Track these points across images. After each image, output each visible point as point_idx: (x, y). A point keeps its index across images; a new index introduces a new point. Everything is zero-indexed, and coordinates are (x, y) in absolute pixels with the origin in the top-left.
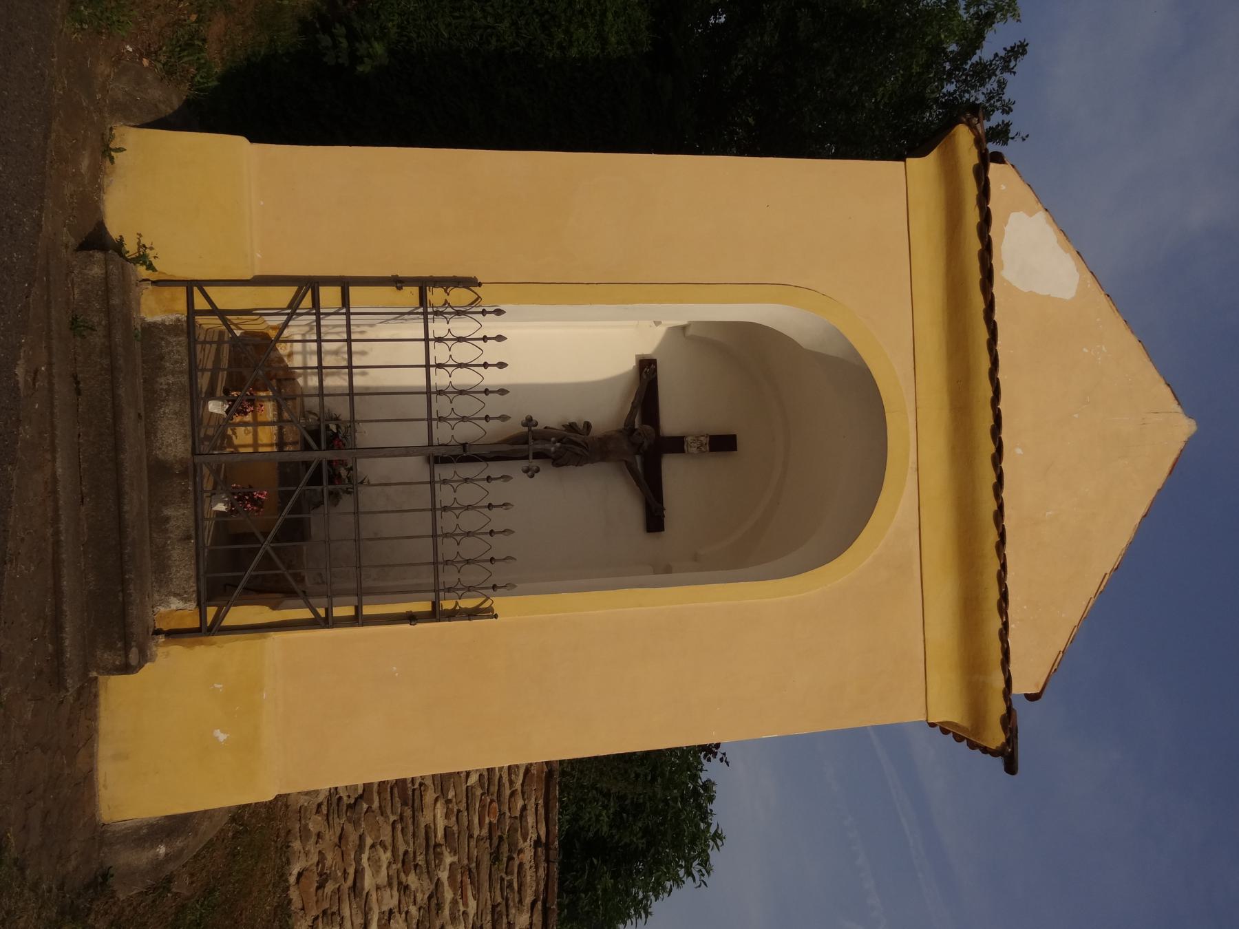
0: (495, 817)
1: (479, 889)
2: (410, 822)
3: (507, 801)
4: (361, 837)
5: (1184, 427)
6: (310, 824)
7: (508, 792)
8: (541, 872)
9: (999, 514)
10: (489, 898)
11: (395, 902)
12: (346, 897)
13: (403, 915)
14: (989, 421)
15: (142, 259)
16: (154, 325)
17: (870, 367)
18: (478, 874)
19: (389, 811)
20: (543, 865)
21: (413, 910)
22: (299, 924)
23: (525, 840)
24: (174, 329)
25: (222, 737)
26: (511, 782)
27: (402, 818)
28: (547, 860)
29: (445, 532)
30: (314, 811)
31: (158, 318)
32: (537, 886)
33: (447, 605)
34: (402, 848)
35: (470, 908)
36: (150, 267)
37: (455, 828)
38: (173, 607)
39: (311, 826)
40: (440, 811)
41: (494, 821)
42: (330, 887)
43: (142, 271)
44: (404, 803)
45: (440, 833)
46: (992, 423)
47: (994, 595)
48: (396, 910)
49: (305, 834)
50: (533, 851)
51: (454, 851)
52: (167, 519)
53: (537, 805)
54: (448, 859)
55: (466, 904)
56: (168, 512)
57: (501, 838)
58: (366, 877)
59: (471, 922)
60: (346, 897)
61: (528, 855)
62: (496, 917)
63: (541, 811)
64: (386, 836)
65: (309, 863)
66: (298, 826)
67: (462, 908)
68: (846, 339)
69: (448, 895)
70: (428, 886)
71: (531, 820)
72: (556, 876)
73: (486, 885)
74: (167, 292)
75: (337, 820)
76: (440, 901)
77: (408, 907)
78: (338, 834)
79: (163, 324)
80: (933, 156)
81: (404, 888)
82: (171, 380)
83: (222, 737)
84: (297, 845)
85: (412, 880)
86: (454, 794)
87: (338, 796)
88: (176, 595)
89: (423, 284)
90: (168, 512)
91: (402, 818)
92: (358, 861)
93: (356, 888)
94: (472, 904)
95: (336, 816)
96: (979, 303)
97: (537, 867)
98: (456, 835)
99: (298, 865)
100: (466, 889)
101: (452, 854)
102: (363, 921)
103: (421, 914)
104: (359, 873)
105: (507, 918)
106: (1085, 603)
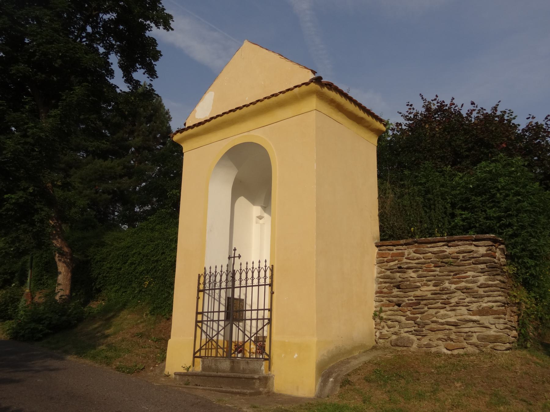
0: (431, 265)
1: (462, 271)
2: (428, 301)
3: (426, 260)
4: (433, 322)
5: (247, 45)
6: (424, 343)
7: (423, 260)
8: (460, 243)
9: (268, 98)
10: (468, 266)
11: (464, 309)
12: (459, 330)
13: (469, 304)
14: (232, 113)
15: (188, 369)
16: (202, 367)
17: (224, 153)
18: (455, 271)
19: (422, 310)
20: (456, 243)
21: (467, 300)
22: (469, 351)
23: (445, 251)
24: (203, 362)
25: (296, 355)
26: (418, 259)
27: (426, 305)
28: (454, 241)
29: (251, 283)
30: (419, 341)
31: (201, 366)
32: (466, 244)
33: (268, 281)
34: (439, 305)
35: (471, 274)
36: (190, 367)
37: (433, 282)
38: (264, 369)
39: (425, 343)
40: (425, 288)
41: (433, 265)
42: (453, 336)
43: (190, 370)
44: (419, 304)
45: (434, 288)
46: (232, 112)
47: (274, 99)
48: (467, 308)
49: (428, 346)
50: (452, 247)
51: (442, 282)
52: (243, 368)
53: (431, 247)
54: (447, 285)
55: (468, 277)
56: (242, 368)
57: (442, 262)
58: (450, 320)
59: (478, 274)
60: (459, 330)
61: (453, 249)
62: (477, 263)
63: (432, 245)
64: (433, 311)
65: (443, 345)
66: (424, 348)
67: (471, 278)
68: (218, 162)
69: (463, 284)
70: (459, 293)
71: (435, 249)
72: (461, 236)
73: (461, 268)
74: (196, 363)
75: (424, 332)
76: (464, 288)
77: (466, 302)
78: (430, 332)
79: (202, 365)
80: (182, 145)
81: (458, 304)
82: (213, 364)
83: (296, 355)
84: (433, 350)
85: (453, 301)
86: (418, 283)
87: (414, 331)
88: (261, 368)
89: (199, 291)
90: (242, 368)
91: (426, 305)
92: (442, 324)
93: (455, 325)
94: (469, 273)
95: (422, 332)
96: (207, 124)
97: (458, 245)
98: (436, 281)
99: (443, 349)
100: (461, 276)
101: (444, 283)
102: (472, 323)
103: (469, 296)
104: (448, 323)
105: (480, 257)
106: (287, 62)
